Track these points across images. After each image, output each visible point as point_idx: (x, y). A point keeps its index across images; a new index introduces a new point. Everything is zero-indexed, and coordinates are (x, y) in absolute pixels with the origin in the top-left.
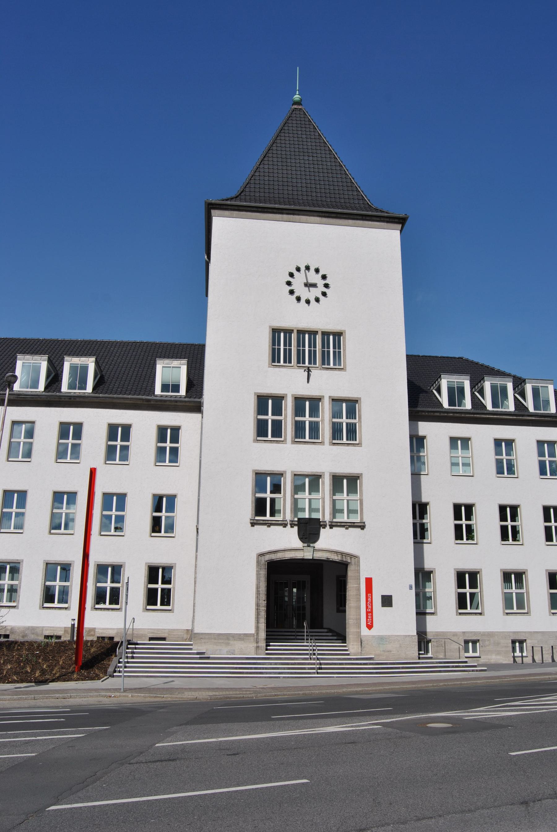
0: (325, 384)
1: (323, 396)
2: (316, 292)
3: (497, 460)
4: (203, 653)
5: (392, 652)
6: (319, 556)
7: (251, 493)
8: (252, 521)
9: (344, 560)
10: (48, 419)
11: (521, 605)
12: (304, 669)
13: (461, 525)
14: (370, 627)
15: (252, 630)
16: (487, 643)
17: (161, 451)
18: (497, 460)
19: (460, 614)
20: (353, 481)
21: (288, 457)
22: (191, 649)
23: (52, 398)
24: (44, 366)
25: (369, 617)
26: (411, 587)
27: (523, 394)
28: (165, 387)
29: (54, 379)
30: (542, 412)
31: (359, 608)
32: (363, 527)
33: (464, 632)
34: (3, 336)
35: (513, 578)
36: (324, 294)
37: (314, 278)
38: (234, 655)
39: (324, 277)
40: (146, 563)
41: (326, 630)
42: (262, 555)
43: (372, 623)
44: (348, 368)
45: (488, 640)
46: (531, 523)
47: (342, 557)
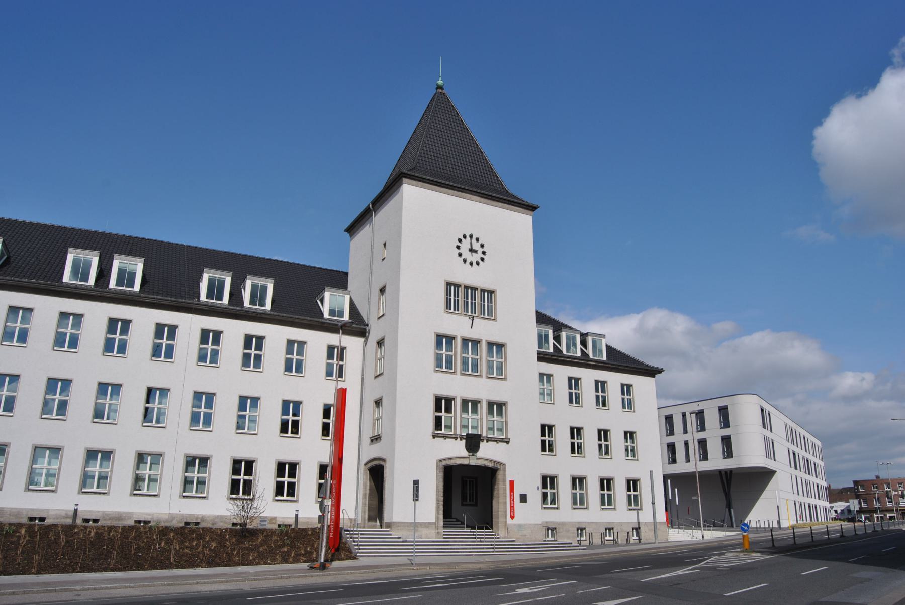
2: (476, 257)
3: (328, 364)
10: (97, 314)
11: (553, 501)
14: (512, 517)
17: (246, 357)
18: (287, 360)
19: (277, 500)
20: (501, 406)
23: (100, 293)
24: (228, 281)
26: (538, 488)
27: (559, 342)
28: (332, 312)
29: (103, 274)
31: (505, 503)
32: (508, 443)
34: (6, 216)
35: (578, 482)
36: (482, 259)
37: (476, 246)
39: (482, 246)
42: (441, 461)
46: (31, 395)
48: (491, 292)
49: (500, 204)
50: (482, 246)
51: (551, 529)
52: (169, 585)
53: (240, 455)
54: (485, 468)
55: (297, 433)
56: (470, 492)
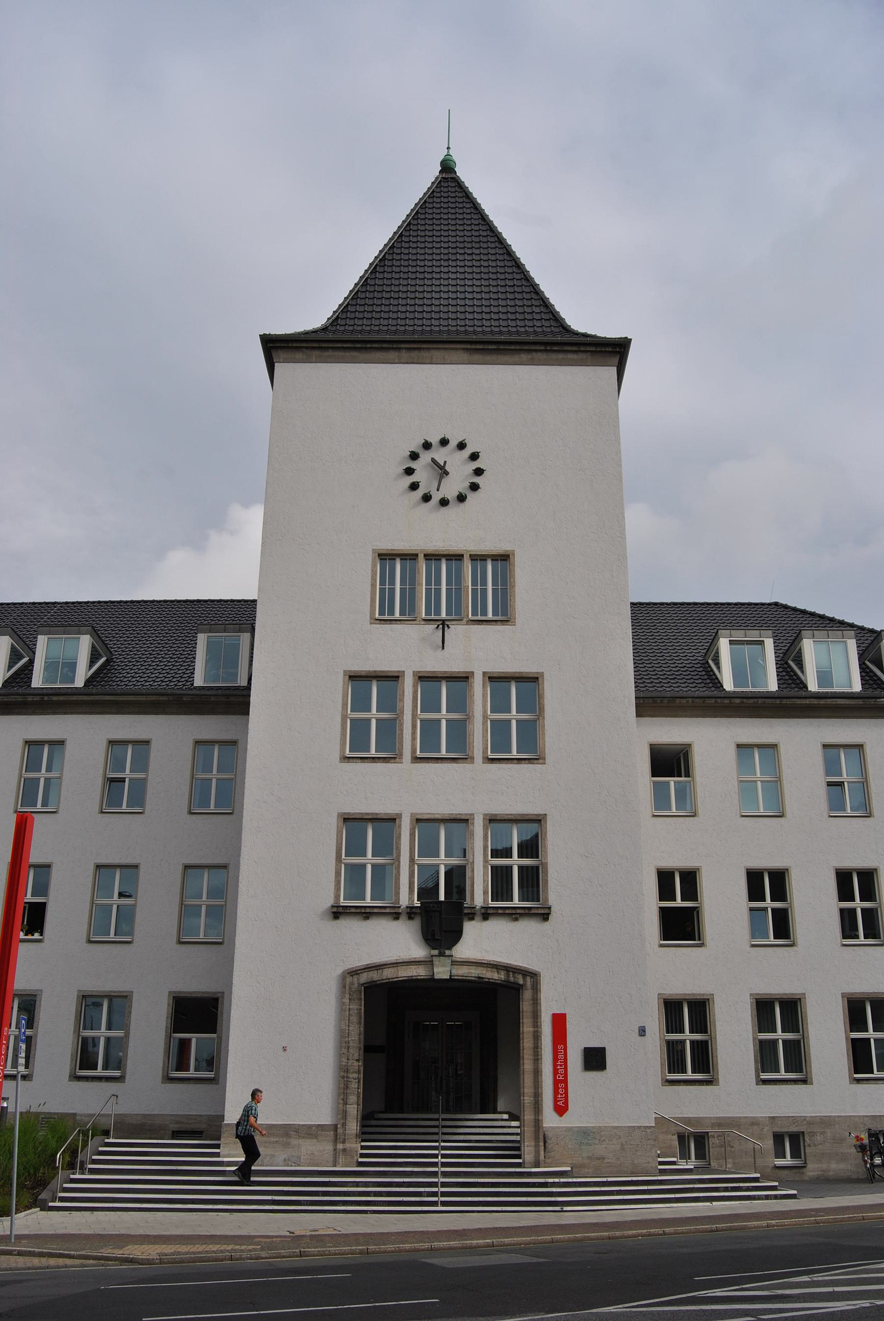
0: (477, 650)
1: (473, 673)
5: (606, 1161)
6: (461, 972)
8: (335, 910)
9: (512, 979)
12: (419, 1194)
13: (854, 910)
14: (561, 1109)
15: (324, 1116)
16: (819, 1138)
19: (765, 1082)
21: (407, 789)
22: (217, 1155)
25: (560, 1091)
26: (642, 1032)
28: (51, 666)
30: (751, 689)
33: (773, 1118)
38: (299, 1165)
39: (414, 456)
40: (170, 993)
41: (506, 1116)
42: (354, 972)
43: (566, 1102)
45: (823, 1133)
46: (815, 904)
47: (508, 975)
48: (503, 559)
49: (524, 357)
50: (414, 456)
51: (696, 1141)
52: (222, 1260)
56: (439, 1048)
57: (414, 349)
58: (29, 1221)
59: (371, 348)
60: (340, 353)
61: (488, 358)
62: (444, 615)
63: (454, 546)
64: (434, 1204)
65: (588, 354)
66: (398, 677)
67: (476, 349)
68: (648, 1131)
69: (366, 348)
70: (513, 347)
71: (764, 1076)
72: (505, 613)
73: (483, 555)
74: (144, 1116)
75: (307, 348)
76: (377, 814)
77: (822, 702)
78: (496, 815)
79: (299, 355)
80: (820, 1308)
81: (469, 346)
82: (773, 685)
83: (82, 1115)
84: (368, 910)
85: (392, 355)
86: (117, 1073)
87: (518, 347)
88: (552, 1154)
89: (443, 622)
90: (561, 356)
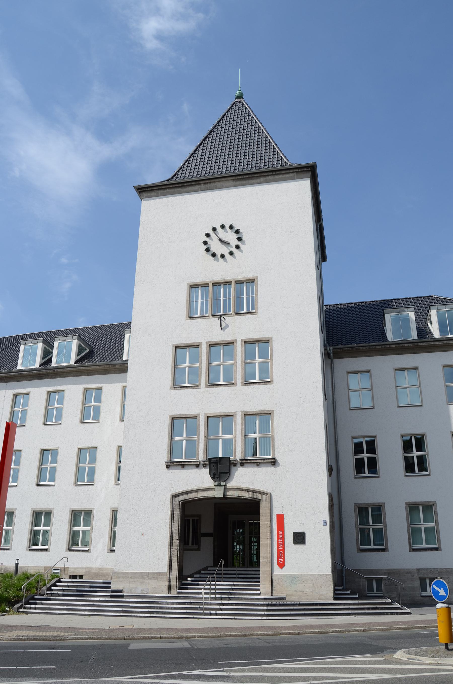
0: (241, 328)
1: (236, 340)
4: (121, 592)
6: (230, 494)
7: (167, 436)
8: (167, 464)
9: (255, 497)
12: (197, 609)
14: (282, 565)
19: (414, 550)
26: (325, 523)
42: (175, 496)
44: (260, 311)
47: (253, 495)
49: (262, 179)
53: (78, 506)
54: (240, 501)
55: (375, 472)
57: (207, 183)
58: (12, 619)
59: (187, 185)
60: (172, 190)
61: (244, 182)
62: (222, 313)
63: (227, 278)
64: (200, 614)
65: (295, 173)
66: (199, 345)
67: (238, 179)
68: (328, 576)
69: (184, 186)
70: (256, 175)
71: (415, 547)
72: (253, 309)
73: (242, 281)
74: (99, 569)
75: (156, 190)
76: (188, 415)
77: (441, 343)
78: (247, 412)
79: (153, 194)
80: (354, 678)
81: (234, 178)
82: (414, 336)
83: (71, 568)
84: (183, 463)
85: (197, 187)
86: (87, 548)
87: (258, 175)
88: (276, 588)
89: (221, 316)
90: (281, 176)
